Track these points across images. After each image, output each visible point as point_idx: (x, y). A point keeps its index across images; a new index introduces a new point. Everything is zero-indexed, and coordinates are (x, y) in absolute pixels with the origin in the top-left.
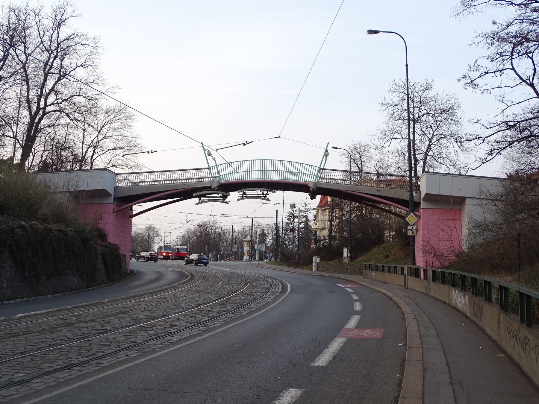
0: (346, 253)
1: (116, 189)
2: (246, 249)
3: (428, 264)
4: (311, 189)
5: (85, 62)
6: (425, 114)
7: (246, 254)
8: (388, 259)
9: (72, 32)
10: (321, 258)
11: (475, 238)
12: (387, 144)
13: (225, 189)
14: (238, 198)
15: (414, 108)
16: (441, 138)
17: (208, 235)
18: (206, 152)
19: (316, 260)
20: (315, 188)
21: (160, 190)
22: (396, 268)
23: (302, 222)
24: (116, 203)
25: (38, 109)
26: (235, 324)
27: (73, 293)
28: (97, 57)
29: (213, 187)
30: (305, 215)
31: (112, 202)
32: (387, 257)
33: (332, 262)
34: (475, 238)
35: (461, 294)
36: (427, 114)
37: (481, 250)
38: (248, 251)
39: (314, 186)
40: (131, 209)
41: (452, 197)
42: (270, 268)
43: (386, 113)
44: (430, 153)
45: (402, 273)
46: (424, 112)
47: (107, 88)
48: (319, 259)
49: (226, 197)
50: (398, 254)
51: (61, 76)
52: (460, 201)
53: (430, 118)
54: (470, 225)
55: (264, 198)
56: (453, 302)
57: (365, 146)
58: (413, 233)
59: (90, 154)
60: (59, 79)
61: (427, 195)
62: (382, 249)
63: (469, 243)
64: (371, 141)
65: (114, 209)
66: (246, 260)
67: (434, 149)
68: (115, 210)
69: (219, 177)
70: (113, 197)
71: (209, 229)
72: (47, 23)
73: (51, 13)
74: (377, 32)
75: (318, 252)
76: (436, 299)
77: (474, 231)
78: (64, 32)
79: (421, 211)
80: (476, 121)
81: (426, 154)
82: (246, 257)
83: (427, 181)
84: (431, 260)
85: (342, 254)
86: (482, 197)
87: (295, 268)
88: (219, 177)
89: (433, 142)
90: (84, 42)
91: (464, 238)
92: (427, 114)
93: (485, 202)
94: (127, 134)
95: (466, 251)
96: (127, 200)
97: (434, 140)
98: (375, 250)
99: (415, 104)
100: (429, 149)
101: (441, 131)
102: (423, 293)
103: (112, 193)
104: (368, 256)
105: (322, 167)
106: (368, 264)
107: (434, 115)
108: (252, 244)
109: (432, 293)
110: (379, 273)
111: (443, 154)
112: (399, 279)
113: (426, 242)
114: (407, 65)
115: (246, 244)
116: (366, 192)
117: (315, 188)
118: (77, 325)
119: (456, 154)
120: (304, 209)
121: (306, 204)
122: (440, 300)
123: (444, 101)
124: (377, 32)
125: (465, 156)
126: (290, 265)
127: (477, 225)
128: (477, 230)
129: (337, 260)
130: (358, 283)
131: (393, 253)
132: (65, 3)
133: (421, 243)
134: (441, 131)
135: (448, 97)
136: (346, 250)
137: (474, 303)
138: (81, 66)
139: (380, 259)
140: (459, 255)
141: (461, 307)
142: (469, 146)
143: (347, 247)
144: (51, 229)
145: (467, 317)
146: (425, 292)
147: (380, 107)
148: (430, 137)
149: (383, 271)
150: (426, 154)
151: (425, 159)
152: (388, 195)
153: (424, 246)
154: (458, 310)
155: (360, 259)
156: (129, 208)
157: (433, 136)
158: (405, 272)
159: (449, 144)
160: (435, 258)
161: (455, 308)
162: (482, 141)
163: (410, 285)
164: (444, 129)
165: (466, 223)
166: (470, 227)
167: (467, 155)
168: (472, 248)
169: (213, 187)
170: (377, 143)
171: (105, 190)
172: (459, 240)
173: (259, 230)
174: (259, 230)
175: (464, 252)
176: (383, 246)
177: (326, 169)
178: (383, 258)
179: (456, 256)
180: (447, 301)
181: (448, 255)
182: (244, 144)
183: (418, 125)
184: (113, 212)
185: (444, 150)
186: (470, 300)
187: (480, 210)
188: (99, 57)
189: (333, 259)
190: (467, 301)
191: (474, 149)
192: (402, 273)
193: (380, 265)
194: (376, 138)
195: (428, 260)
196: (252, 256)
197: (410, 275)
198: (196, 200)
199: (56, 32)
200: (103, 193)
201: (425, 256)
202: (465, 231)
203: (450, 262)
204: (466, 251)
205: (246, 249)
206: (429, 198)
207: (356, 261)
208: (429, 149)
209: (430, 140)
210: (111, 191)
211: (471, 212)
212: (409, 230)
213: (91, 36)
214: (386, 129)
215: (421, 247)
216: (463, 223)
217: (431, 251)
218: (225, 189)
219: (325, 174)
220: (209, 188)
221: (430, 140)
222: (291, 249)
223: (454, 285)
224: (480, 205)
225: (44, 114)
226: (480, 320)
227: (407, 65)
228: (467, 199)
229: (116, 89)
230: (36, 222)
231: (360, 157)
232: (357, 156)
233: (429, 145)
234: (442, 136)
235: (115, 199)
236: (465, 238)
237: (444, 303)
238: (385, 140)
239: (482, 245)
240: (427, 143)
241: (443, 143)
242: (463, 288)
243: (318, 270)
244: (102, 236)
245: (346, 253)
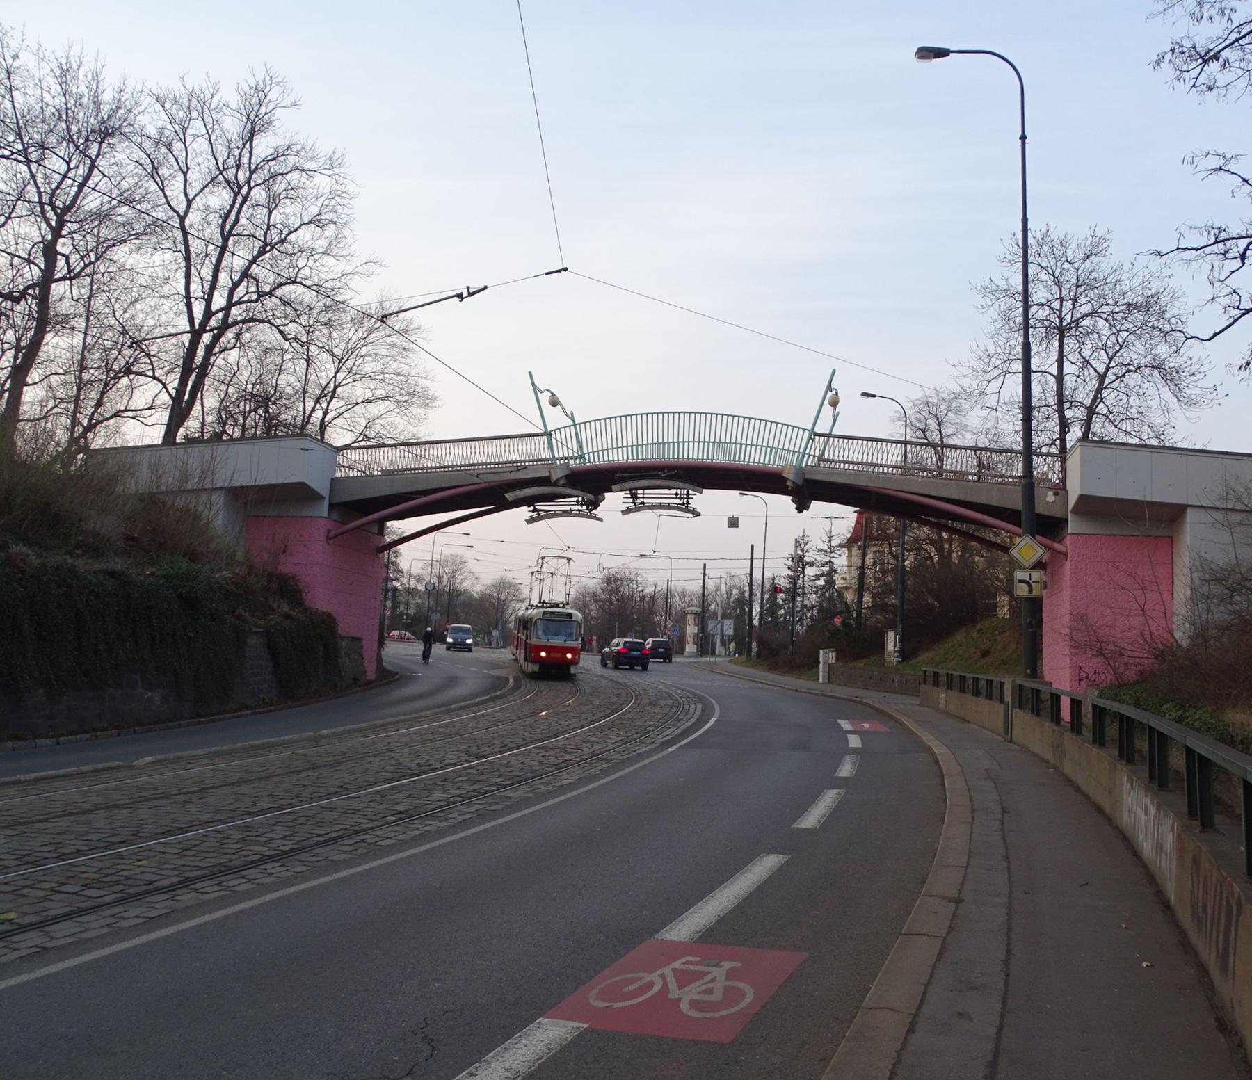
0: (891, 642)
1: (335, 482)
2: (691, 630)
3: (1083, 675)
4: (789, 483)
5: (319, 214)
6: (1087, 315)
7: (690, 640)
8: (988, 660)
9: (285, 142)
10: (838, 652)
11: (1208, 610)
12: (994, 387)
13: (590, 483)
14: (624, 507)
15: (1062, 300)
16: (1129, 371)
17: (624, 601)
18: (545, 398)
19: (827, 657)
20: (800, 482)
21: (435, 486)
22: (976, 680)
23: (822, 575)
24: (335, 516)
25: (208, 313)
26: (428, 846)
27: (135, 732)
28: (345, 202)
29: (554, 478)
30: (827, 559)
31: (325, 513)
32: (985, 654)
33: (860, 664)
34: (1208, 610)
35: (1146, 801)
36: (1093, 314)
37: (1225, 640)
38: (696, 635)
39: (796, 474)
40: (381, 532)
41: (1148, 502)
42: (730, 674)
43: (993, 313)
44: (1101, 408)
45: (1002, 700)
46: (1086, 309)
47: (355, 264)
48: (834, 655)
49: (595, 505)
50: (1013, 647)
51: (266, 245)
52: (1173, 515)
53: (1101, 323)
54: (1195, 575)
55: (686, 508)
56: (1125, 819)
57: (950, 401)
58: (1030, 591)
59: (319, 414)
60: (262, 252)
61: (1082, 498)
62: (975, 635)
63: (1194, 624)
64: (955, 378)
65: (329, 531)
66: (692, 655)
67: (1109, 396)
68: (333, 533)
69: (581, 457)
70: (326, 503)
71: (624, 590)
72: (233, 126)
73: (234, 100)
74: (942, 53)
75: (833, 640)
76: (1078, 789)
77: (1206, 590)
78: (263, 146)
79: (1068, 540)
80: (1216, 162)
81: (1091, 411)
82: (690, 647)
83: (1084, 462)
84: (1092, 664)
85: (882, 645)
86: (1230, 506)
87: (783, 674)
88: (581, 457)
89: (1106, 382)
90: (307, 166)
91: (1181, 609)
92: (1093, 314)
93: (1236, 518)
94: (405, 369)
95: (1185, 643)
96: (368, 511)
97: (1110, 377)
98: (960, 636)
99: (1064, 292)
100: (1097, 397)
101: (1128, 355)
102: (1047, 762)
103: (324, 491)
104: (942, 651)
105: (822, 428)
106: (930, 669)
107: (1110, 318)
108: (703, 618)
109: (1068, 769)
110: (955, 694)
111: (1134, 411)
112: (988, 712)
113: (1080, 618)
114: (1023, 138)
115: (690, 619)
116: (927, 493)
117: (800, 482)
118: (82, 818)
119: (1166, 411)
120: (825, 548)
121: (830, 537)
122: (1087, 797)
123: (1137, 282)
124: (942, 53)
125: (1188, 414)
126: (774, 667)
127: (1217, 576)
128: (1217, 590)
129: (873, 659)
130: (896, 720)
131: (1000, 646)
132: (268, 78)
133: (1066, 620)
134: (1128, 355)
135: (1147, 271)
136: (891, 636)
137: (1196, 862)
138: (310, 222)
139: (970, 658)
140: (1165, 653)
141: (1147, 848)
142: (1197, 391)
143: (893, 626)
144: (72, 569)
145: (1167, 907)
146: (1052, 760)
147: (979, 300)
148: (1101, 369)
149: (963, 690)
150: (1091, 411)
151: (1088, 423)
152: (984, 501)
153: (1073, 629)
154: (1136, 854)
155: (924, 657)
156: (376, 530)
157: (1108, 368)
158: (1008, 697)
159: (1147, 385)
160: (1101, 660)
161: (1127, 841)
162: (1238, 263)
163: (1017, 733)
164: (1137, 352)
165: (1186, 572)
166: (1196, 580)
167: (1192, 413)
168: (1201, 634)
169: (554, 478)
170: (971, 383)
171: (302, 484)
172: (1167, 615)
173: (735, 592)
174: (735, 592)
175: (1179, 646)
176: (978, 627)
177: (839, 437)
178: (978, 654)
179: (1156, 657)
180: (1106, 806)
181: (1136, 654)
182: (460, 296)
183: (1071, 344)
184: (328, 538)
185: (1134, 401)
186: (1180, 844)
187: (1225, 536)
188: (352, 201)
189: (864, 657)
190: (1169, 841)
191: (1211, 397)
192: (1002, 700)
193: (942, 671)
194: (967, 371)
195: (1083, 666)
196: (705, 646)
197: (1020, 707)
198: (524, 512)
199: (248, 146)
200: (300, 494)
201: (1077, 654)
202: (1182, 592)
203: (1141, 672)
204: (1185, 643)
205: (691, 630)
206: (1090, 506)
207: (913, 662)
208: (1097, 397)
209: (1102, 378)
210: (323, 488)
211: (1198, 541)
212: (1020, 581)
213: (324, 150)
214: (991, 352)
215: (1067, 631)
216: (1176, 570)
217: (1087, 640)
218: (590, 483)
219: (836, 451)
220: (545, 481)
221: (1102, 378)
222: (772, 633)
223: (1127, 755)
224: (1228, 526)
225: (224, 326)
226: (1224, 958)
227: (1023, 138)
228: (1189, 511)
229: (373, 267)
230: (24, 549)
231: (939, 424)
232: (932, 423)
233: (1100, 389)
234: (1131, 368)
235: (332, 506)
236: (1182, 611)
237: (1099, 809)
238: (988, 377)
239: (1227, 628)
240: (1093, 385)
241: (1132, 383)
242: (1159, 779)
243: (830, 681)
244: (289, 589)
245: (891, 642)
